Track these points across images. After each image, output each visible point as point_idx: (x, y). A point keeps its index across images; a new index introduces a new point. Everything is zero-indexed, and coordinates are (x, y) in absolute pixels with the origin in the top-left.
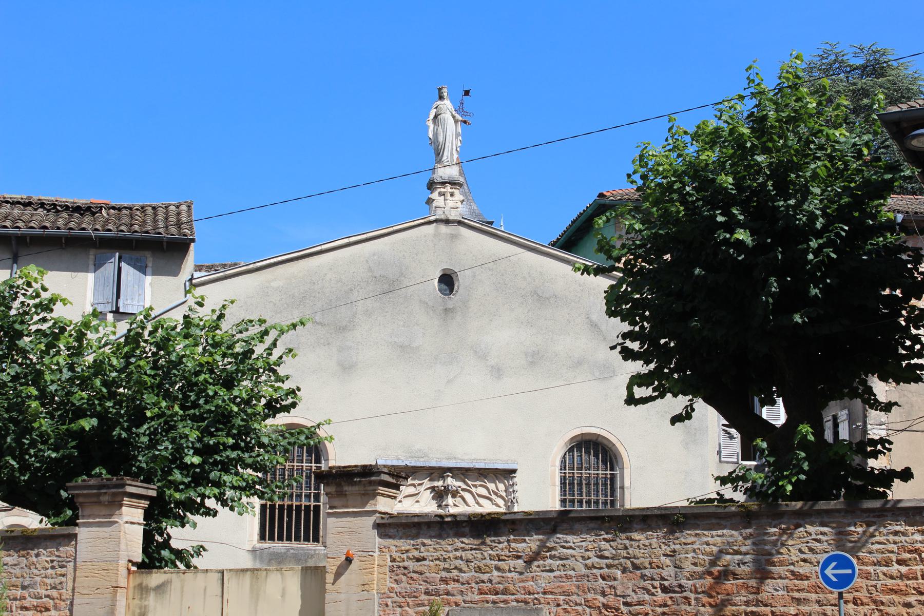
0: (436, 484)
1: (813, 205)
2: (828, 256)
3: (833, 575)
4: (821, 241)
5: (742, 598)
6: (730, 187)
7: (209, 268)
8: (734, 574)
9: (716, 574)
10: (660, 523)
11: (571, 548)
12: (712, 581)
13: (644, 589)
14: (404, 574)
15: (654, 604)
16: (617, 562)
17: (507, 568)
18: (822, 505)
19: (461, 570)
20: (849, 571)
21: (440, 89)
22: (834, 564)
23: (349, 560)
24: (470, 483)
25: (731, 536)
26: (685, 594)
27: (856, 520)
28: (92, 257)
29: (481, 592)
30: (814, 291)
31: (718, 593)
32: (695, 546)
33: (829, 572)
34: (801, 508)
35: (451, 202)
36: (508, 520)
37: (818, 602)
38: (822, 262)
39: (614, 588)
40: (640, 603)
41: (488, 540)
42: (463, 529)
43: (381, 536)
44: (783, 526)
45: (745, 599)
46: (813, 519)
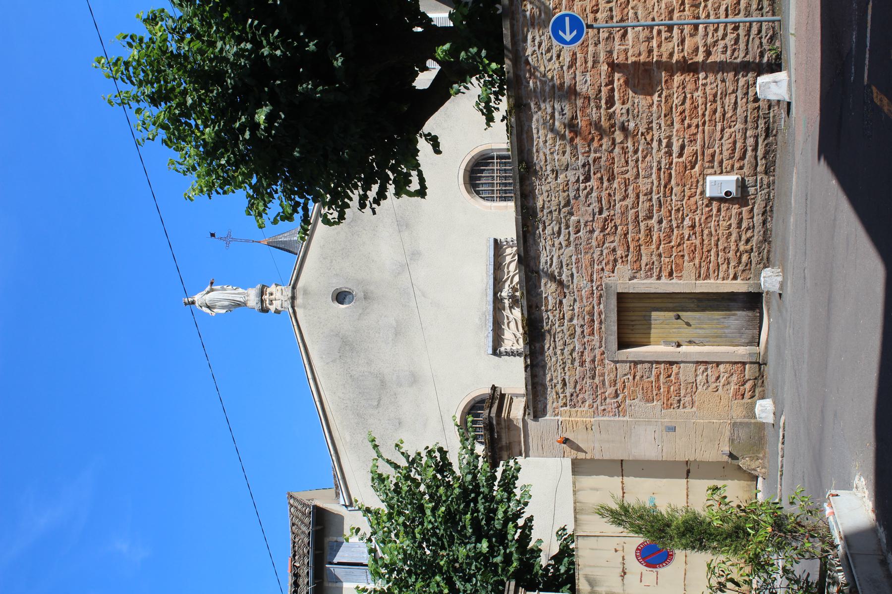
0: (507, 305)
1: (231, 50)
2: (277, 37)
3: (571, 33)
4: (265, 42)
5: (594, 112)
6: (217, 128)
7: (337, 495)
8: (572, 118)
9: (572, 134)
10: (528, 182)
11: (551, 259)
12: (578, 138)
13: (587, 197)
14: (577, 396)
15: (600, 188)
16: (563, 220)
17: (570, 312)
18: (507, 41)
19: (573, 350)
20: (567, 19)
21: (186, 304)
22: (561, 33)
23: (566, 441)
24: (506, 277)
25: (538, 121)
26: (591, 162)
27: (520, 10)
28: (330, 585)
29: (592, 333)
30: (312, 47)
31: (590, 133)
32: (548, 153)
33: (568, 37)
34: (510, 59)
35: (277, 295)
36: (529, 312)
37: (596, 45)
38: (283, 42)
39: (586, 222)
40: (600, 200)
41: (546, 328)
42: (537, 348)
43: (544, 413)
44: (528, 75)
45: (594, 109)
46: (520, 49)
